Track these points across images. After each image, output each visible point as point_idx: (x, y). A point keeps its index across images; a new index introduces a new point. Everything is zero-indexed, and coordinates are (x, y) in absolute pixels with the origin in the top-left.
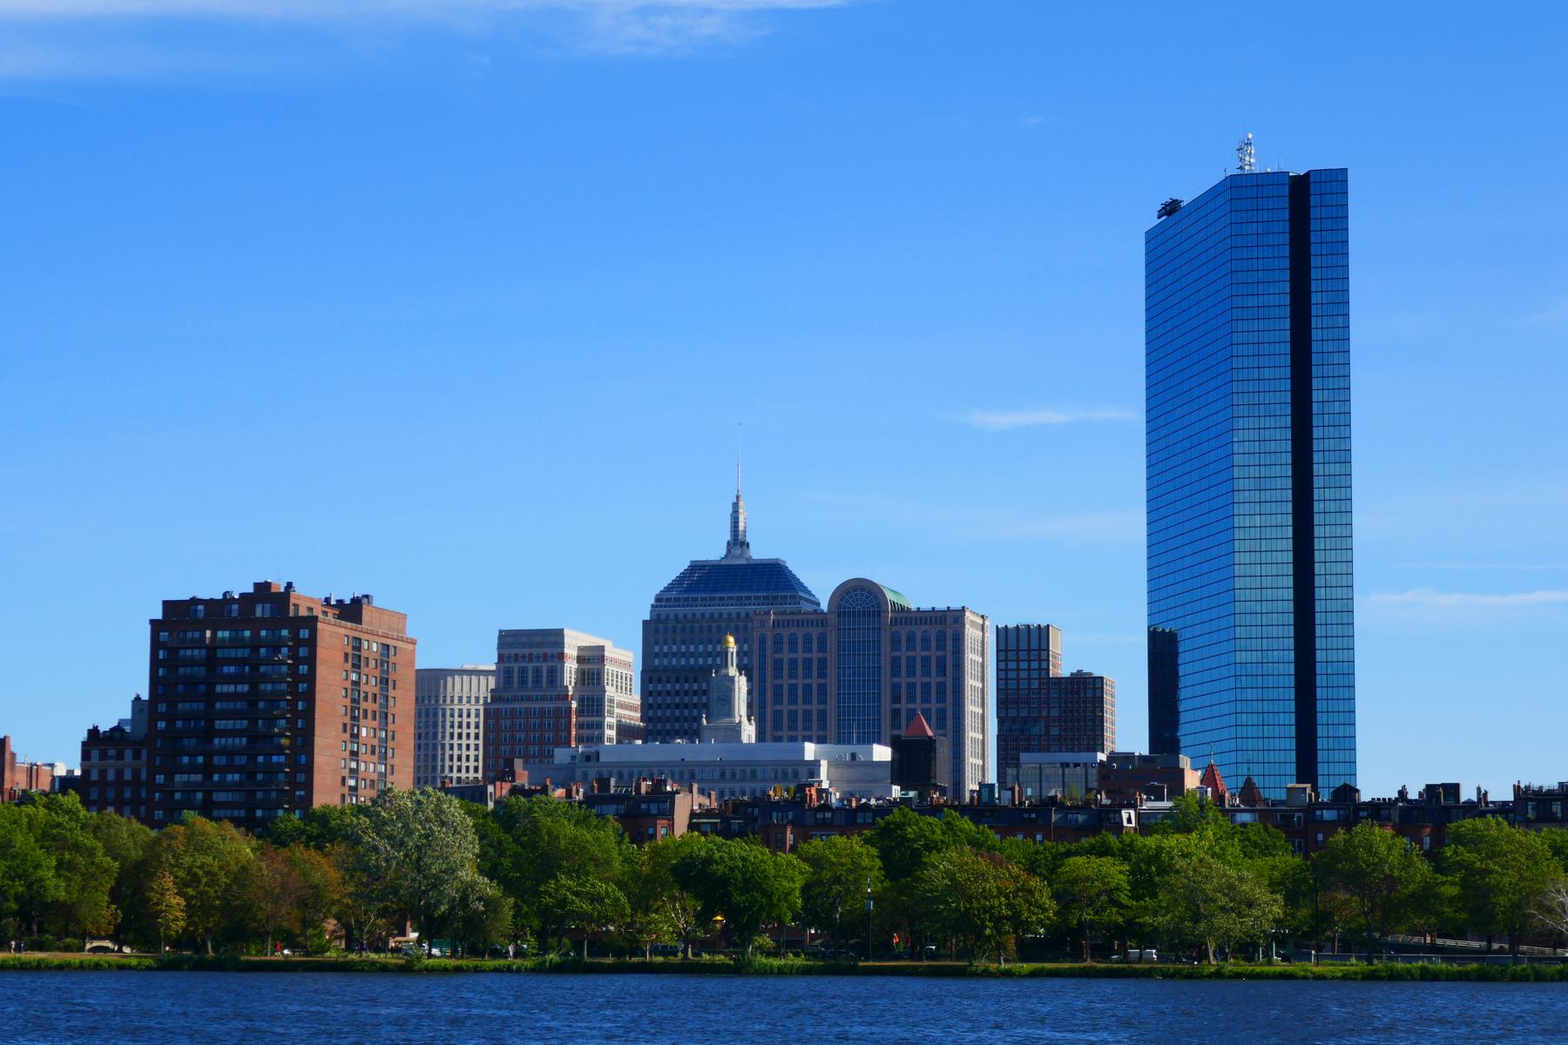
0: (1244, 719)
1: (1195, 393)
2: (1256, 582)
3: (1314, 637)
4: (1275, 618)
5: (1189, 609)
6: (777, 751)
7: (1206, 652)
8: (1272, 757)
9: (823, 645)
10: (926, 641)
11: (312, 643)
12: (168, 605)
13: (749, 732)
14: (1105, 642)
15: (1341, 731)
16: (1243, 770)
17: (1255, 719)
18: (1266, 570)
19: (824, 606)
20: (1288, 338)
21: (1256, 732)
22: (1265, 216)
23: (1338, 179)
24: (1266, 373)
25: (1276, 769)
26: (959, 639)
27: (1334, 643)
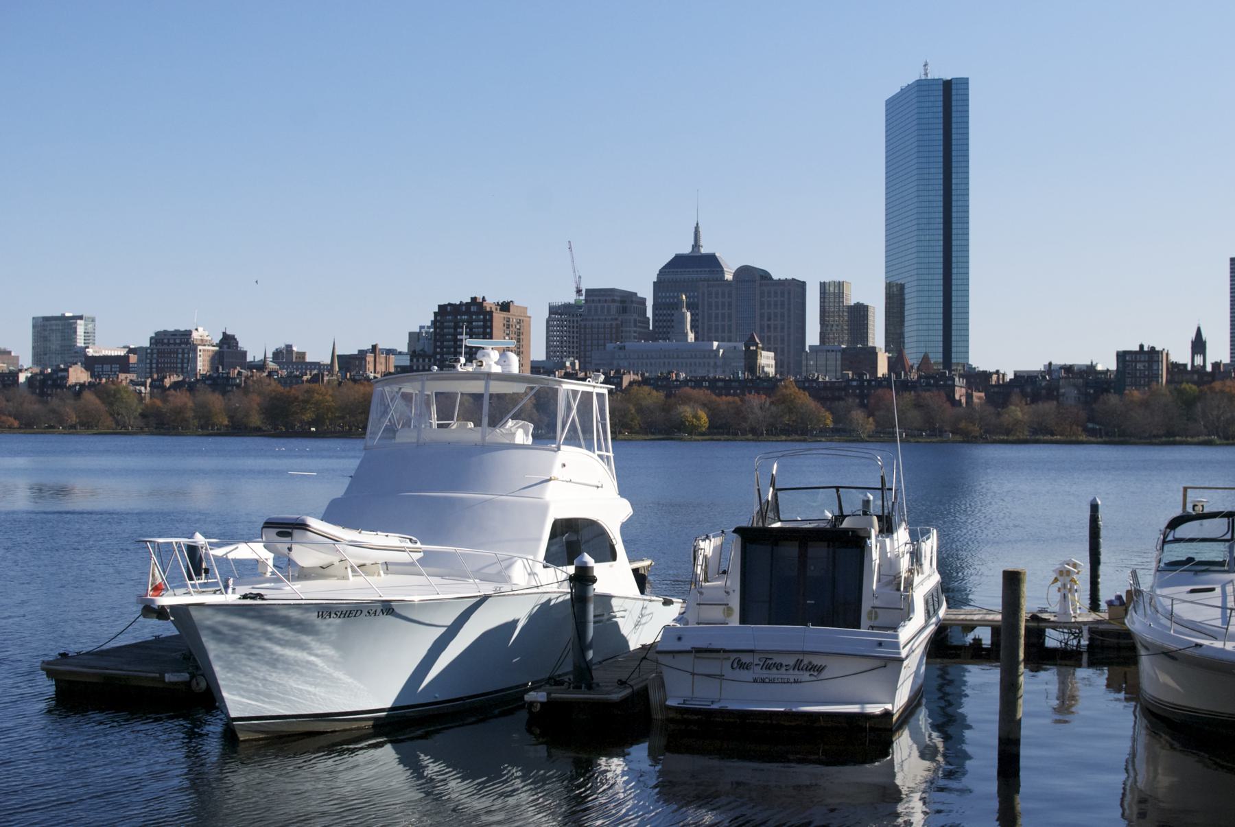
4: (935, 282)
6: (703, 345)
9: (730, 295)
11: (491, 320)
12: (440, 306)
13: (691, 337)
14: (869, 291)
16: (923, 350)
19: (729, 277)
22: (932, 99)
23: (965, 82)
24: (933, 171)
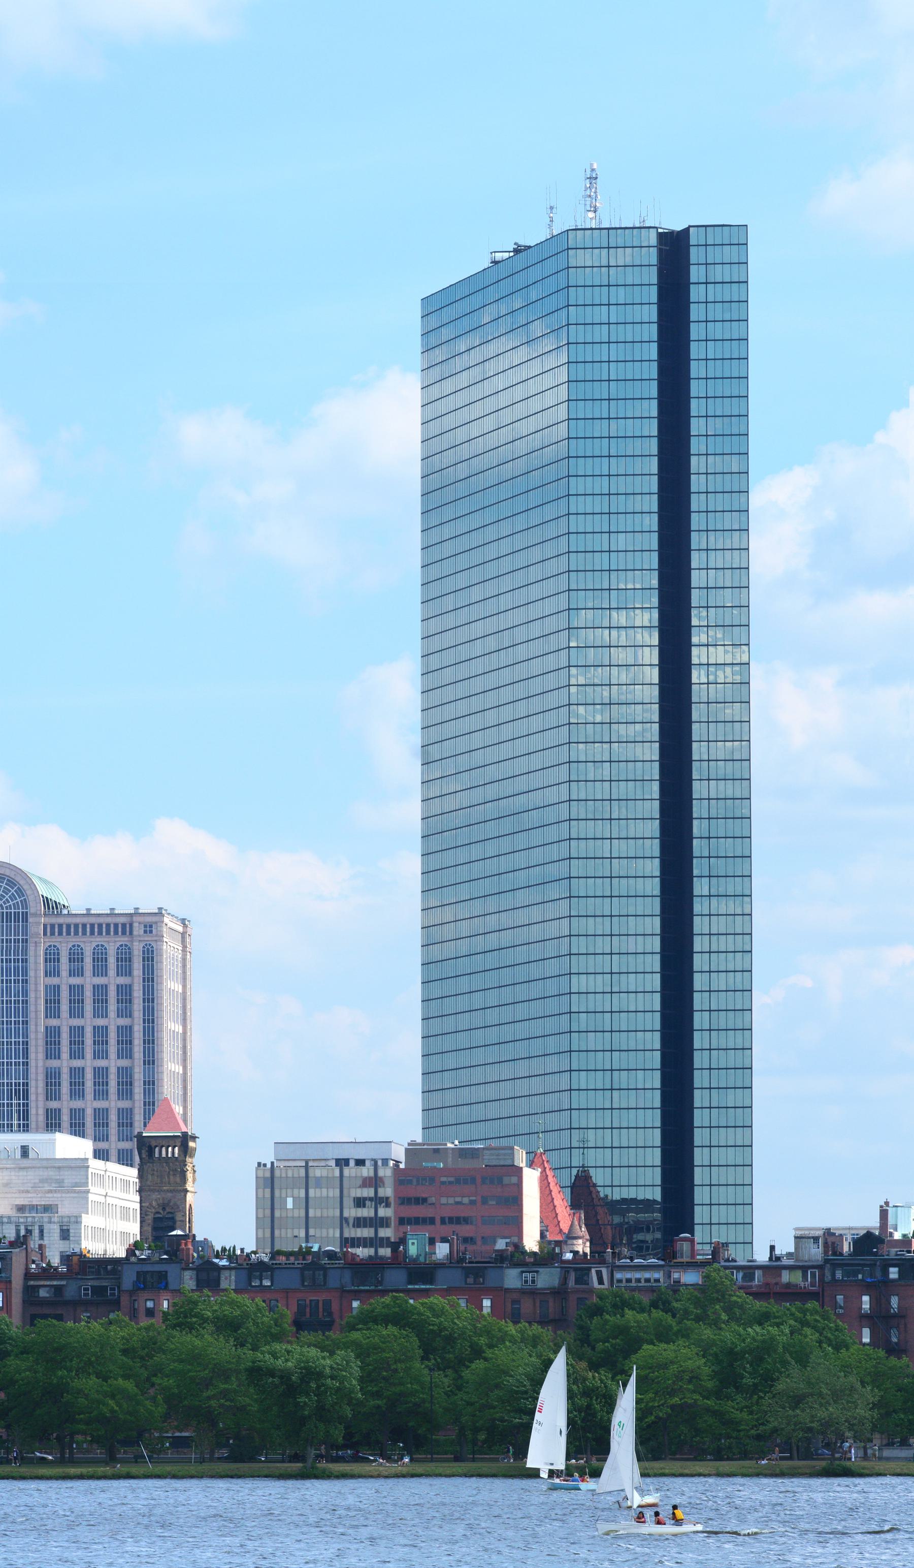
0: (583, 1080)
1: (506, 565)
2: (602, 485)
3: (688, 360)
5: (492, 998)
7: (521, 992)
8: (624, 1138)
10: (100, 960)
15: (731, 1098)
17: (599, 1080)
18: (621, 848)
20: (654, 298)
21: (601, 1100)
25: (631, 1157)
26: (150, 958)
27: (722, 1194)
